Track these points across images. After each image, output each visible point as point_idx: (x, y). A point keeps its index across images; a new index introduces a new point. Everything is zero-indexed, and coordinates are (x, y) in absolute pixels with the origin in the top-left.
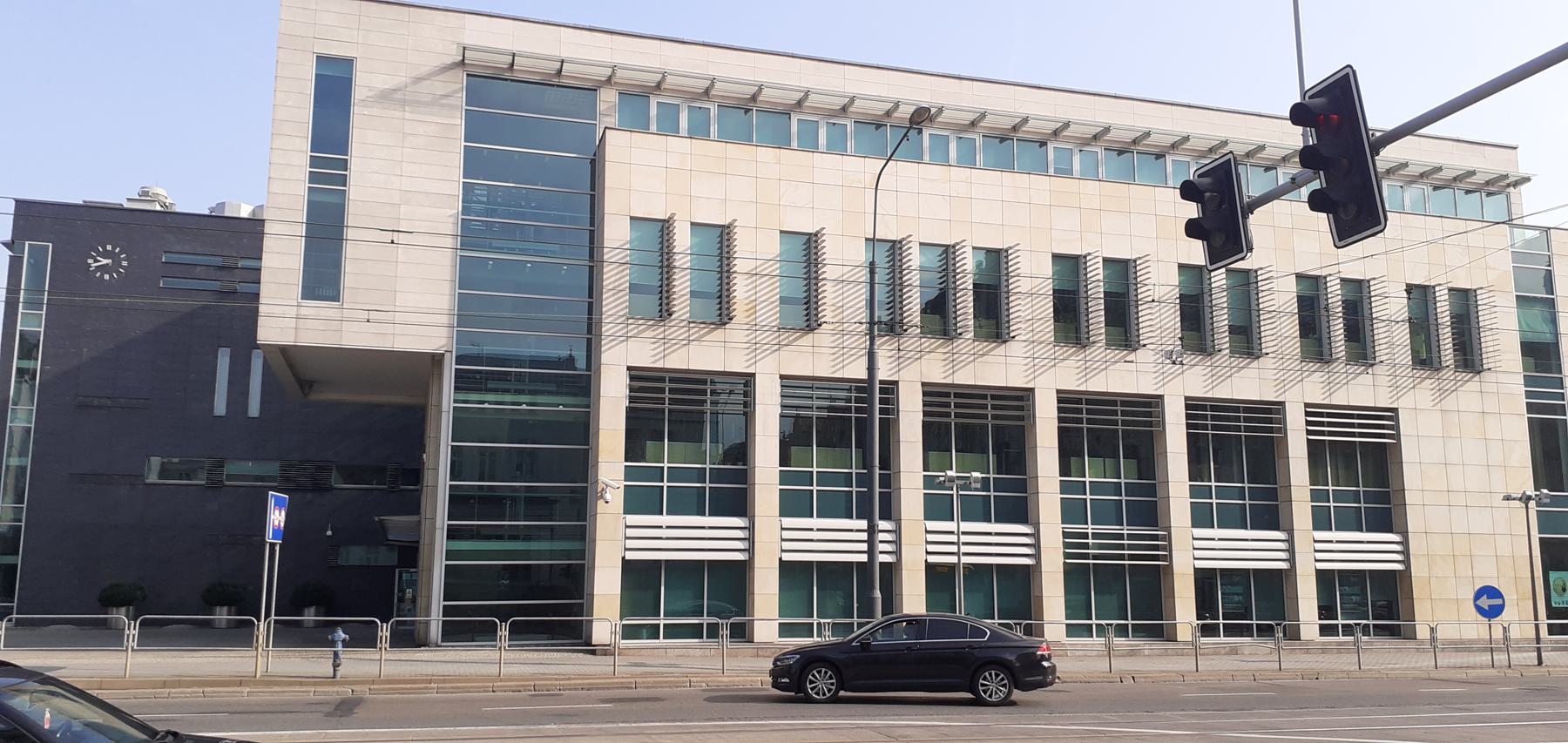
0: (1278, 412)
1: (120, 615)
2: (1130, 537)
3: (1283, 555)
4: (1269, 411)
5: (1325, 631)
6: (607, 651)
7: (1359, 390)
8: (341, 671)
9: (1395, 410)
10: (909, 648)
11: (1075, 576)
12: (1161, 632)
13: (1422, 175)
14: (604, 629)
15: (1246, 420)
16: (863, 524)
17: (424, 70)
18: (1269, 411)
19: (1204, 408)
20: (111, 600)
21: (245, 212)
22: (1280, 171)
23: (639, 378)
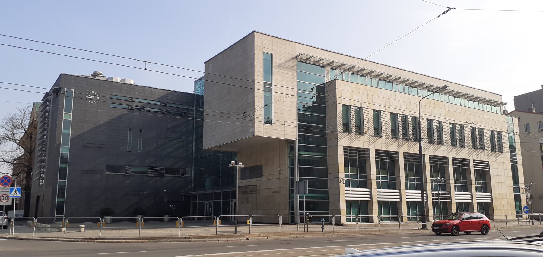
0: (396, 154)
1: (139, 218)
2: (442, 194)
3: (398, 197)
4: (364, 151)
5: (349, 220)
6: (345, 225)
7: (483, 156)
8: (324, 230)
9: (488, 162)
10: (438, 222)
11: (301, 203)
12: (368, 220)
13: (377, 76)
14: (343, 220)
16: (420, 192)
17: (288, 59)
18: (364, 151)
20: (104, 213)
21: (119, 80)
22: (337, 70)
23: (346, 149)
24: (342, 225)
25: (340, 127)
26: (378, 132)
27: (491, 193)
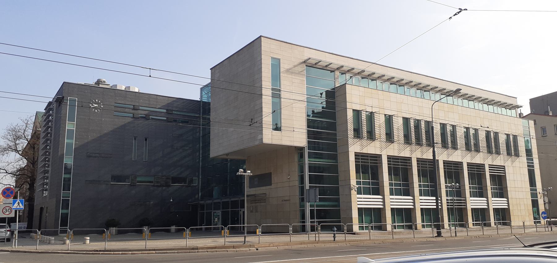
0: (409, 160)
1: (145, 229)
2: (457, 200)
3: (381, 203)
4: (376, 157)
6: (358, 234)
7: (499, 161)
9: (504, 166)
12: (382, 228)
13: (358, 73)
14: (356, 228)
15: (401, 162)
16: (434, 198)
17: (296, 64)
18: (376, 157)
19: (474, 166)
23: (357, 155)
24: (354, 234)
25: (351, 133)
26: (390, 137)
27: (508, 198)
